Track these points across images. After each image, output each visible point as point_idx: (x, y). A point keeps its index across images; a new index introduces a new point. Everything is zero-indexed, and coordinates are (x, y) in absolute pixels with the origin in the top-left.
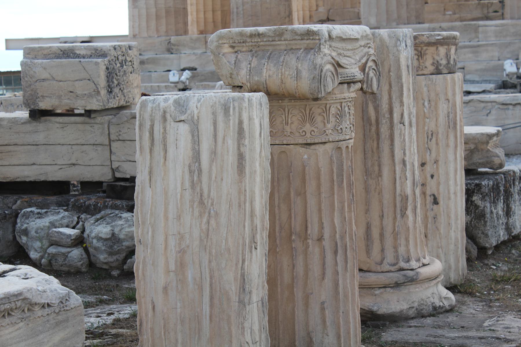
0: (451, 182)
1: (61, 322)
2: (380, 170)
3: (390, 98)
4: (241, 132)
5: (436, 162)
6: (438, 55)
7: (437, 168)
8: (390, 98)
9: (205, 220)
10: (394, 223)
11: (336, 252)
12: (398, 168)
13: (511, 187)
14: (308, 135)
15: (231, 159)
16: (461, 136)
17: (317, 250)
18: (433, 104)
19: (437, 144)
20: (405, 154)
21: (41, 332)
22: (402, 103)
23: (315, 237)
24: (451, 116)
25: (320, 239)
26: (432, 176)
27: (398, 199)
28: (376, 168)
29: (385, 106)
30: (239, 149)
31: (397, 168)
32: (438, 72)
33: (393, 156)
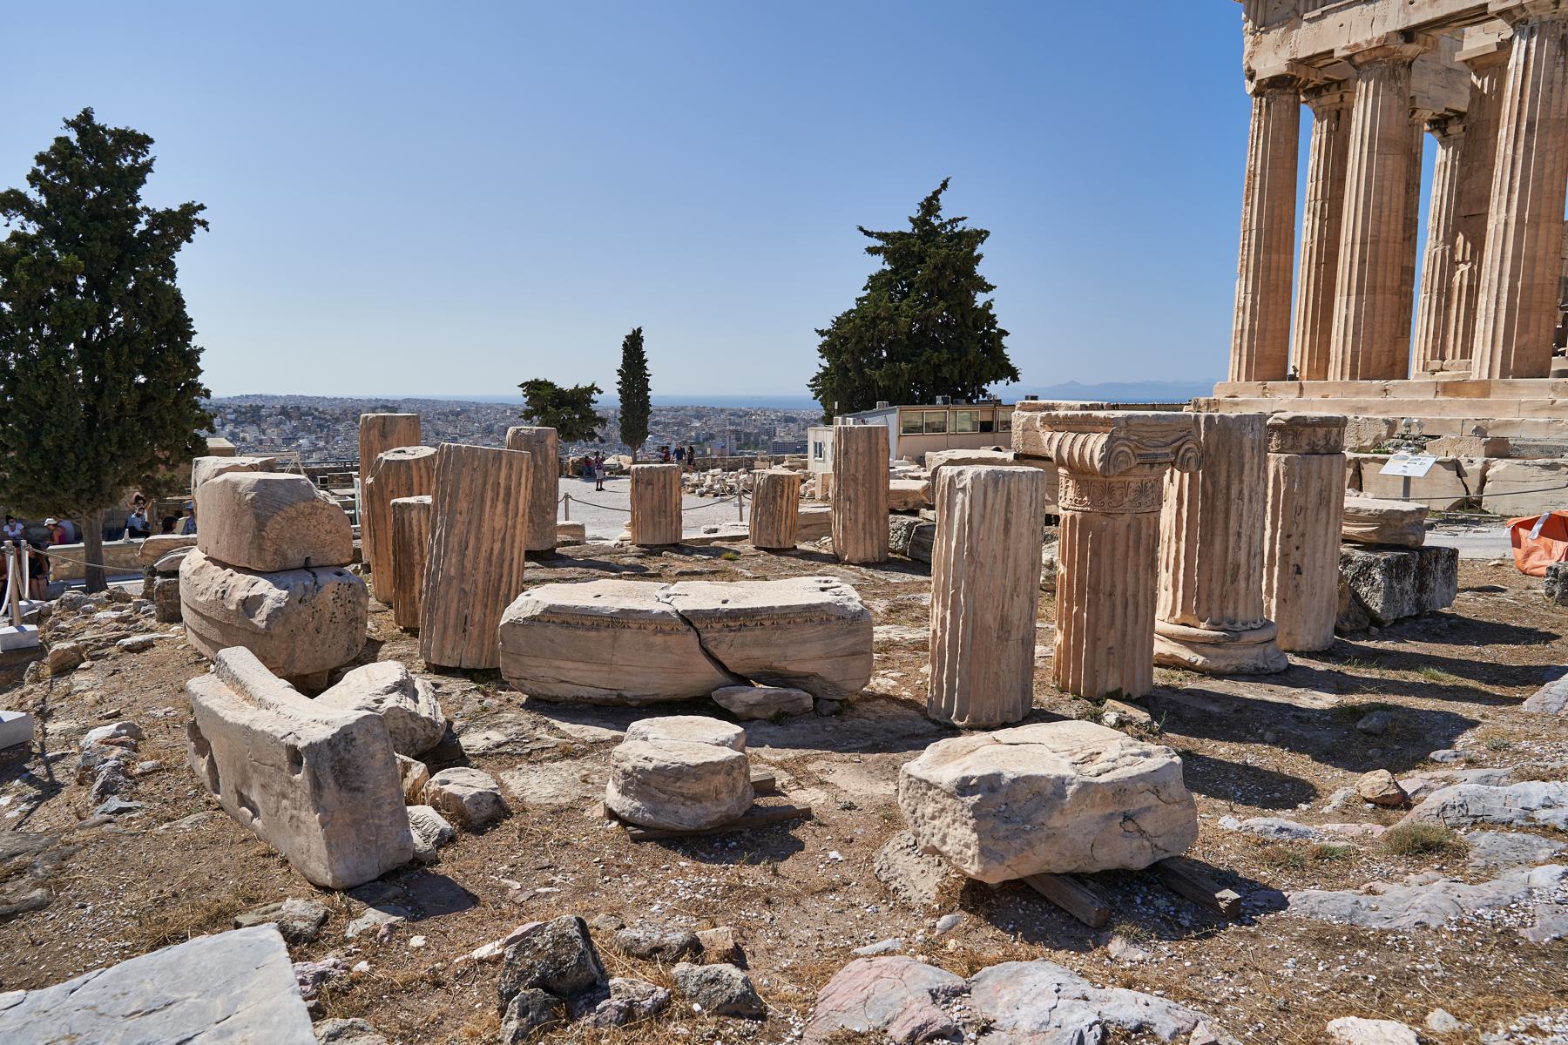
0: (1319, 555)
1: (853, 631)
2: (1212, 540)
3: (1229, 476)
4: (1008, 501)
5: (1303, 535)
6: (1316, 436)
7: (1303, 541)
8: (1229, 476)
9: (973, 568)
10: (1222, 588)
11: (1126, 607)
12: (1232, 540)
13: (1430, 564)
14: (1106, 506)
15: (998, 522)
16: (172, 560)
17: (1107, 603)
18: (1304, 481)
19: (1305, 519)
20: (1240, 527)
21: (836, 636)
22: (1241, 481)
23: (1107, 593)
24: (1324, 494)
25: (1111, 595)
26: (1297, 548)
27: (1230, 567)
28: (1209, 537)
29: (1223, 482)
30: (1006, 515)
31: (1231, 539)
32: (1314, 452)
33: (1226, 528)
